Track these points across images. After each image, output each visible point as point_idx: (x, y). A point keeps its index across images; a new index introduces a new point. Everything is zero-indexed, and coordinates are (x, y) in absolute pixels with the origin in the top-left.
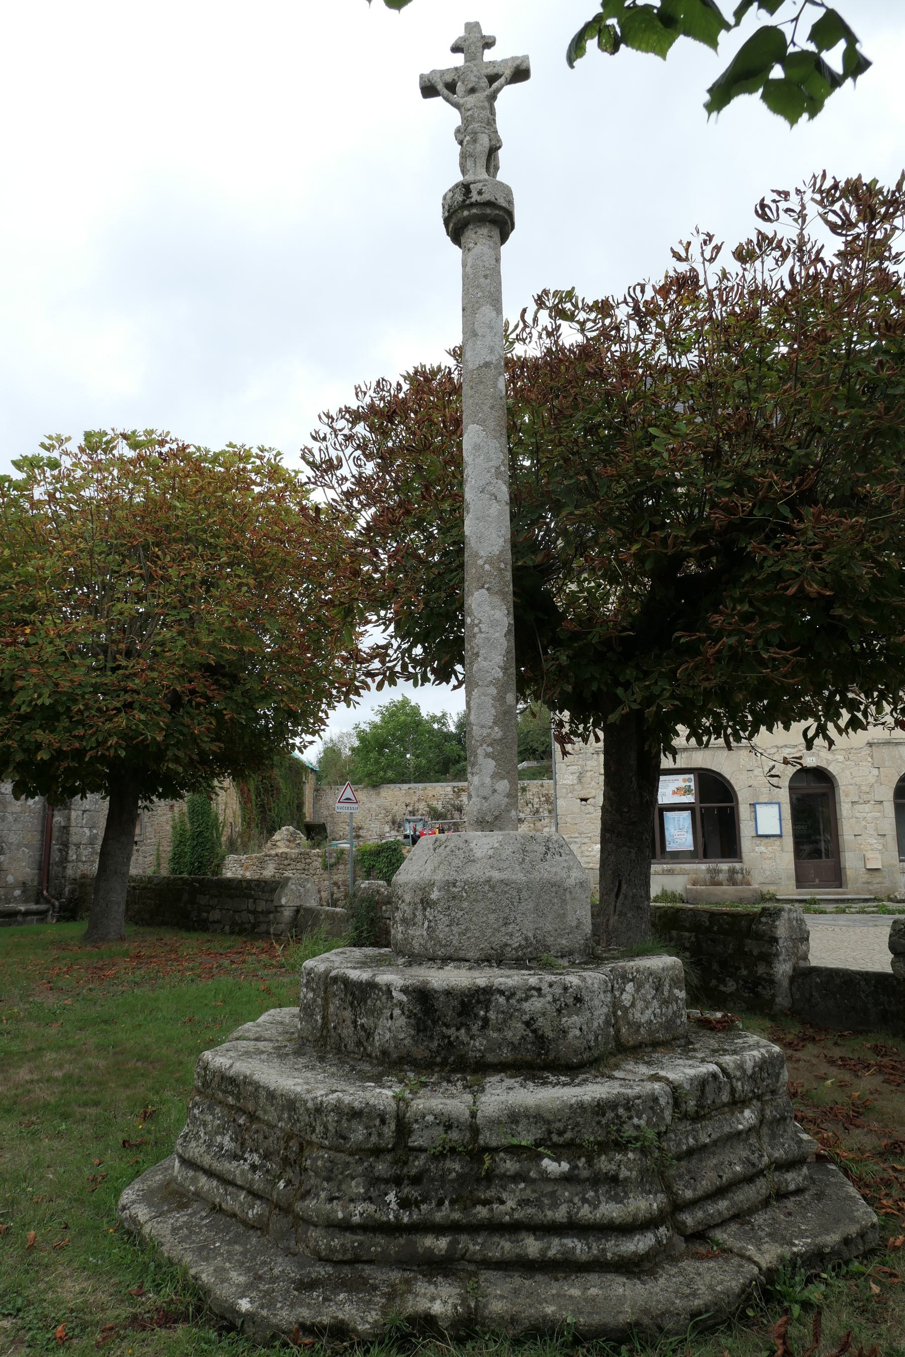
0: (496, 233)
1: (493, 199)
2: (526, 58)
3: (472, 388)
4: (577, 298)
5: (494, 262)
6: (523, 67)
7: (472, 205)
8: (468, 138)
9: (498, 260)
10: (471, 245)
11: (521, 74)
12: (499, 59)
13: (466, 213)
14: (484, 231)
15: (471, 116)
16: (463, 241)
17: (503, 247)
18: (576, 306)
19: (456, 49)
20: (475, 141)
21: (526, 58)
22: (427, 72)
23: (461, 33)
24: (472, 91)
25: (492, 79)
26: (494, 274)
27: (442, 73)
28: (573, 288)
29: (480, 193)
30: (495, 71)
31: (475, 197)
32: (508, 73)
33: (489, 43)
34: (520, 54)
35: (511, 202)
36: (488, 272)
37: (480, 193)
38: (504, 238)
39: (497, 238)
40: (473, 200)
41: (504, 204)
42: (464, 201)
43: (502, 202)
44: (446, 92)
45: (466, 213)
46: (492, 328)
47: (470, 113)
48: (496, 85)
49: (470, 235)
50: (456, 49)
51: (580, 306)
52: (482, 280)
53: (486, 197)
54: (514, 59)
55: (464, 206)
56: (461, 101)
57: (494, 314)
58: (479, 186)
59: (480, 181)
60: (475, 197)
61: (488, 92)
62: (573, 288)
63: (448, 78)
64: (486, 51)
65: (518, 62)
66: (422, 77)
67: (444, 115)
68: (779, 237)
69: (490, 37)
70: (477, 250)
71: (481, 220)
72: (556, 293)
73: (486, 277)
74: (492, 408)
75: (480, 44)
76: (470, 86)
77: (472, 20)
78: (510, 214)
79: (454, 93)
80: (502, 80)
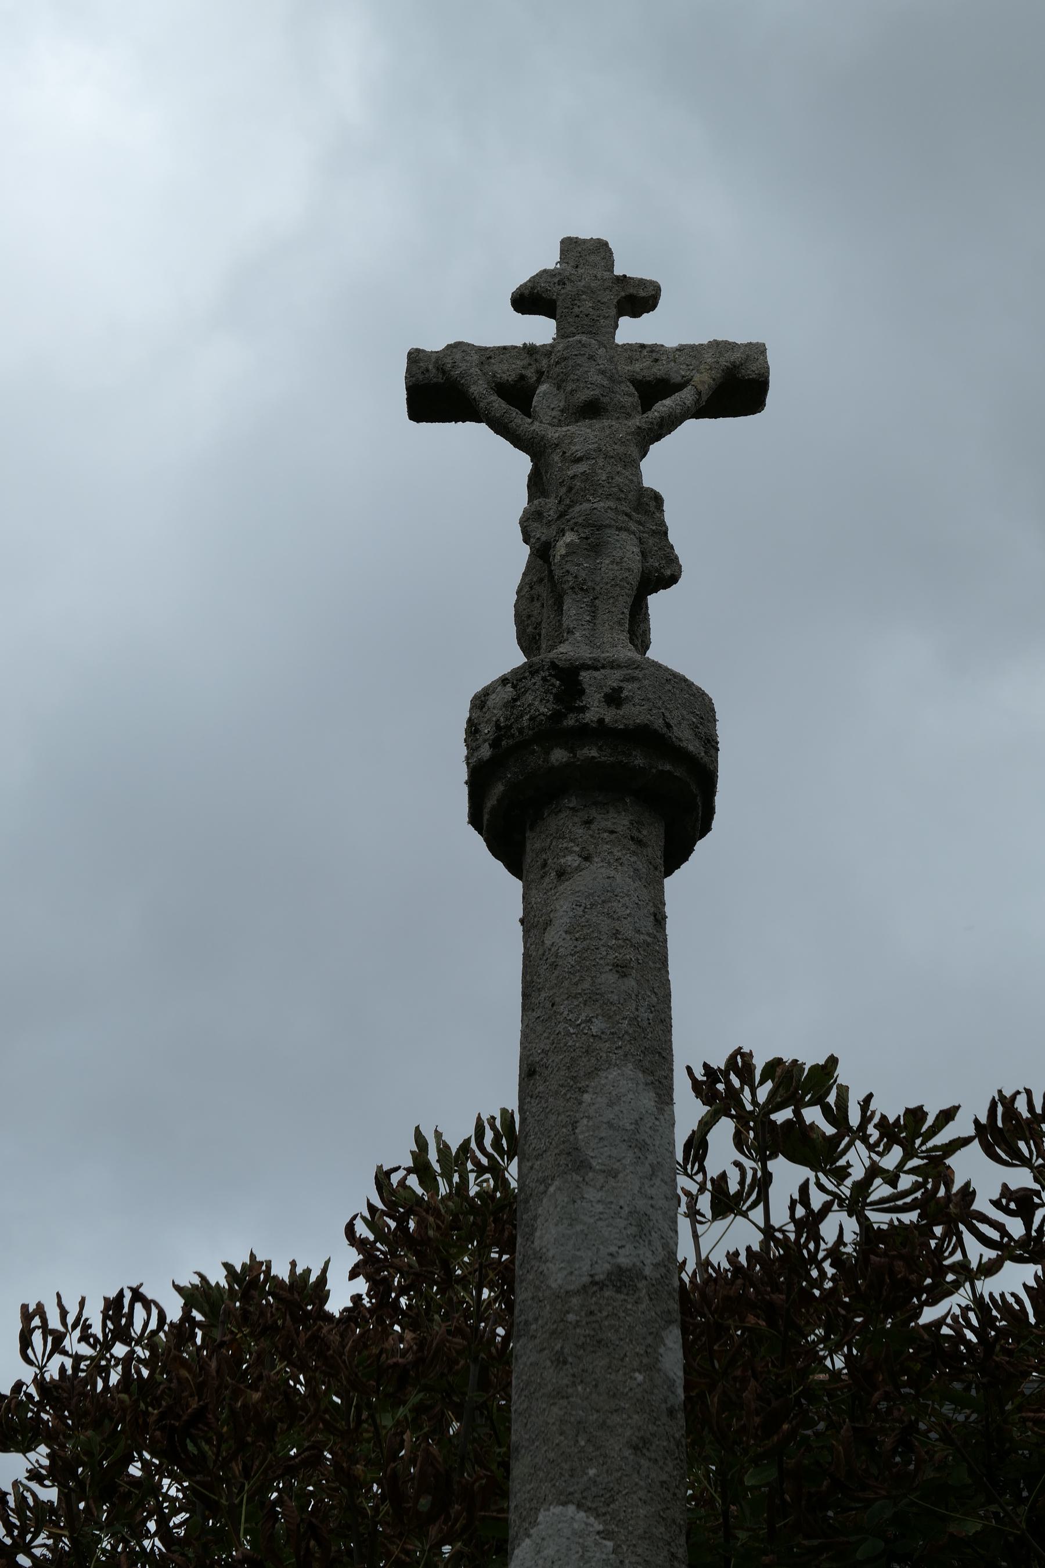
0: (654, 835)
1: (658, 724)
2: (760, 350)
3: (560, 1361)
4: (843, 1093)
5: (649, 924)
6: (751, 371)
7: (585, 733)
8: (569, 537)
9: (659, 920)
10: (572, 860)
11: (737, 386)
12: (671, 342)
13: (559, 756)
14: (621, 821)
15: (586, 477)
16: (534, 843)
17: (667, 881)
18: (837, 1116)
19: (527, 301)
20: (595, 548)
21: (760, 350)
22: (435, 344)
23: (550, 259)
24: (591, 410)
25: (652, 390)
26: (644, 959)
27: (488, 355)
28: (833, 1061)
29: (614, 699)
30: (658, 371)
31: (595, 710)
32: (704, 379)
33: (640, 299)
34: (741, 337)
35: (711, 744)
36: (631, 955)
37: (614, 699)
38: (677, 854)
39: (656, 851)
40: (590, 717)
41: (693, 746)
42: (557, 717)
43: (685, 737)
44: (498, 405)
45: (559, 756)
46: (643, 1147)
47: (582, 468)
48: (664, 406)
49: (566, 830)
50: (527, 301)
51: (854, 1118)
52: (609, 978)
53: (634, 713)
54: (719, 347)
55: (551, 732)
56: (553, 434)
57: (648, 1101)
58: (613, 678)
59: (614, 665)
60: (595, 710)
61: (638, 421)
62: (833, 1061)
63: (507, 371)
64: (624, 321)
65: (736, 356)
66: (415, 357)
67: (484, 470)
68: (485, 1118)
69: (642, 283)
70: (592, 877)
71: (606, 786)
72: (773, 1067)
73: (621, 969)
74: (640, 1446)
75: (611, 298)
76: (583, 396)
77: (586, 232)
78: (706, 779)
79: (526, 410)
80: (687, 395)
